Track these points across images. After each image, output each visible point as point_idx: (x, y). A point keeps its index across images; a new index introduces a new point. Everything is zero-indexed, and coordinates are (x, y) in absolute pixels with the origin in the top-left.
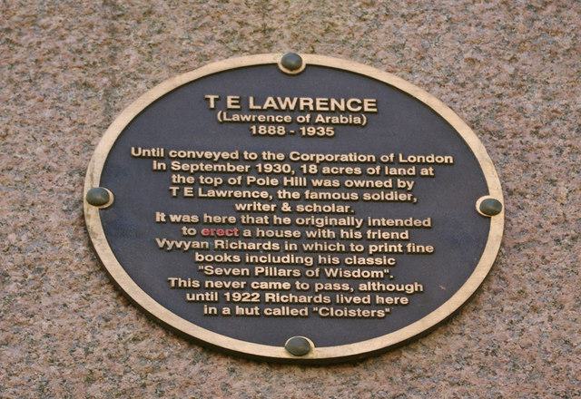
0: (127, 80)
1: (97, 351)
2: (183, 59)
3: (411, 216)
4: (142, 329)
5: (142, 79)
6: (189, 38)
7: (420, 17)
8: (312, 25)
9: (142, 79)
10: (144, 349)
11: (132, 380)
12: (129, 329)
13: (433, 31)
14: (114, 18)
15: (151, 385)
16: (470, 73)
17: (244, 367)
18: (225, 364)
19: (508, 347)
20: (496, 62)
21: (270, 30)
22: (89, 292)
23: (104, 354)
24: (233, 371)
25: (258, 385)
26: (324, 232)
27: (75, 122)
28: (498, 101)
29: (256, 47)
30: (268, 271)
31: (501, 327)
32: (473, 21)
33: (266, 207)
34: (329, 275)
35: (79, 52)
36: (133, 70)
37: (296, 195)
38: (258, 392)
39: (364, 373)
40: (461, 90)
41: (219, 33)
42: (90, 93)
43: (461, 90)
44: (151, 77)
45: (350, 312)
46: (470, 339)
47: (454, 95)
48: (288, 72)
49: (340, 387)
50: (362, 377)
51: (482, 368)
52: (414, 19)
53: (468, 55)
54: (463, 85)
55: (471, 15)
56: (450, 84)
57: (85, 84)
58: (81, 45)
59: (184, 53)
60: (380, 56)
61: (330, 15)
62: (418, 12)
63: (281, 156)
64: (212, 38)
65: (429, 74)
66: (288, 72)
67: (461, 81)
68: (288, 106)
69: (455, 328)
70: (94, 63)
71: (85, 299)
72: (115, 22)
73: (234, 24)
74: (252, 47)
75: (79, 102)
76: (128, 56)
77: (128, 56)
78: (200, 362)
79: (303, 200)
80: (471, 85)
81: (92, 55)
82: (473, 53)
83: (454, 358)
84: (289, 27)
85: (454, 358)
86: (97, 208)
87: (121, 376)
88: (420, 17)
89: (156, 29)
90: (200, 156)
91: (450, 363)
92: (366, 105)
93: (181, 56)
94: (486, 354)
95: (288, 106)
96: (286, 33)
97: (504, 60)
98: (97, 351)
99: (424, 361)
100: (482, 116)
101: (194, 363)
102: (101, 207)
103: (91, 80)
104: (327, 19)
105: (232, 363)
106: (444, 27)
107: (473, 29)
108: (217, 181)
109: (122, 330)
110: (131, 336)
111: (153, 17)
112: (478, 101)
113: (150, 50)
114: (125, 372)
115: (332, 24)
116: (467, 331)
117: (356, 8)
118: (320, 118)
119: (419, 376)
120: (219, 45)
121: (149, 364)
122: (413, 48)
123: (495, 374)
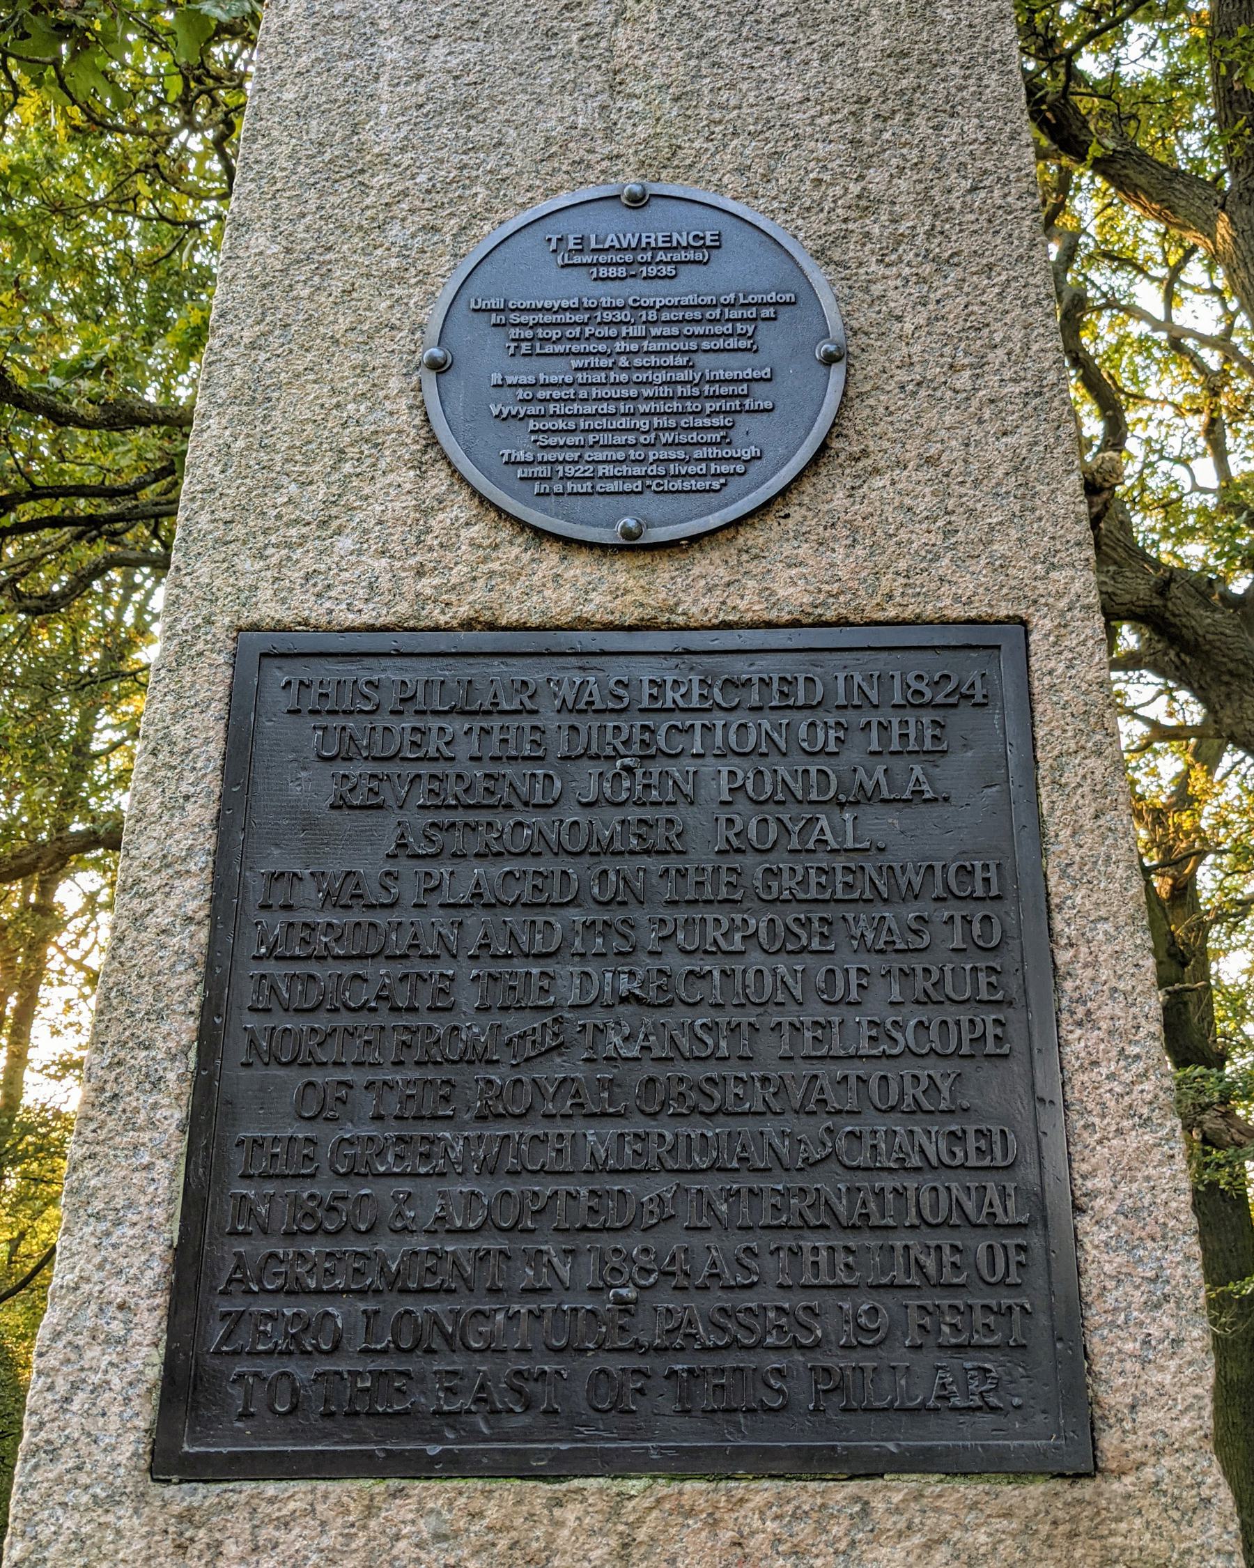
2: (530, 195)
6: (538, 172)
14: (465, 153)
30: (604, 438)
37: (634, 347)
47: (800, 222)
60: (725, 180)
63: (620, 302)
92: (708, 238)
101: (526, 550)
108: (554, 333)
115: (679, 147)
116: (806, 500)
118: (661, 256)
119: (756, 557)
123: (833, 550)
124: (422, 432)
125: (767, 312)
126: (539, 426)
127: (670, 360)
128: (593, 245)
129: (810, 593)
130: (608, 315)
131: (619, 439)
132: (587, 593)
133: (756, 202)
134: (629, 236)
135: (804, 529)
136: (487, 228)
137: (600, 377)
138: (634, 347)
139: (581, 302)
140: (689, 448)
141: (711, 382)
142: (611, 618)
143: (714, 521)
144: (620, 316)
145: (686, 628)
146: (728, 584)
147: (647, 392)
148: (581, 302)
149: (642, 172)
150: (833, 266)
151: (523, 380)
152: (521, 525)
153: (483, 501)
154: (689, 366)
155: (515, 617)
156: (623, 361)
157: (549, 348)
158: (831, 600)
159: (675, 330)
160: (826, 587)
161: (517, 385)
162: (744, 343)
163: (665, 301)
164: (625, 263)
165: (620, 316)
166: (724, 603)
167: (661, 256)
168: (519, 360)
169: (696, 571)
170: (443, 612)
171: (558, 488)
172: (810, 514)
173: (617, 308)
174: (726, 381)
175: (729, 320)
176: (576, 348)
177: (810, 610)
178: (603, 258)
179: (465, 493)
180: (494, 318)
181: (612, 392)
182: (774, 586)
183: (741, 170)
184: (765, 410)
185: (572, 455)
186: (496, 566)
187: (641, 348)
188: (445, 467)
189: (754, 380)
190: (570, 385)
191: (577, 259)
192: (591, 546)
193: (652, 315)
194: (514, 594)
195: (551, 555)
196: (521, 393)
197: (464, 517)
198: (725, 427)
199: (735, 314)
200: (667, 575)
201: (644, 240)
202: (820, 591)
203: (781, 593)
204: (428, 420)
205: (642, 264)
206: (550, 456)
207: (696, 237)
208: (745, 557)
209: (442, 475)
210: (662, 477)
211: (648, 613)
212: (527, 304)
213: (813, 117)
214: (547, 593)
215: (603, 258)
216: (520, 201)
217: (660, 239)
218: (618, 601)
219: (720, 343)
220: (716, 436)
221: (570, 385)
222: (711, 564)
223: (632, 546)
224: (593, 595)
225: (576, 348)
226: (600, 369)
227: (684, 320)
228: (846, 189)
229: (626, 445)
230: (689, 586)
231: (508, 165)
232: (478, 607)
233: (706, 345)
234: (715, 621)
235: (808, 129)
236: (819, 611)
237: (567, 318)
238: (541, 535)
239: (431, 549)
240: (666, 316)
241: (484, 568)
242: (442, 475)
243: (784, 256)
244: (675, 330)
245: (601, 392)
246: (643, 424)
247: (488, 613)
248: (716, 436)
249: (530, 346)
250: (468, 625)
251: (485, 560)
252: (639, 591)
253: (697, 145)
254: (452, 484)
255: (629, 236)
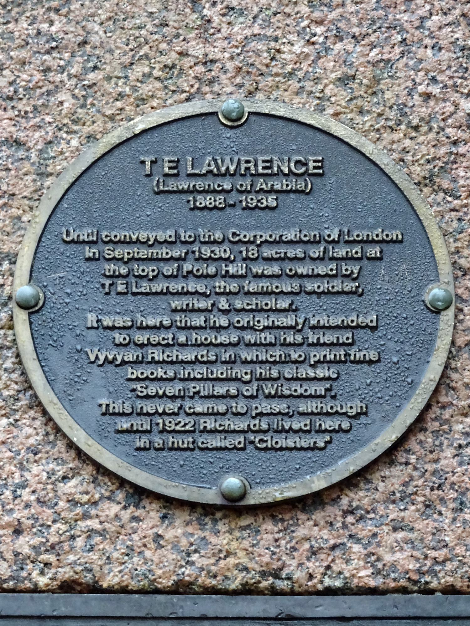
0: (59, 134)
1: (26, 494)
2: (119, 104)
3: (379, 226)
4: (71, 465)
5: (75, 132)
6: (126, 77)
7: (373, 38)
8: (258, 53)
9: (75, 132)
10: (73, 491)
11: (61, 532)
12: (58, 464)
13: (385, 57)
14: (48, 52)
15: (79, 536)
16: (424, 111)
17: (178, 512)
18: (158, 508)
19: (454, 479)
20: (455, 97)
21: (213, 61)
22: (17, 417)
23: (33, 498)
24: (164, 517)
25: (192, 535)
26: (263, 335)
27: (5, 192)
28: (454, 150)
29: (196, 86)
30: (204, 389)
31: (449, 452)
32: (427, 41)
33: (202, 304)
34: (267, 391)
35: (11, 98)
36: (66, 121)
37: (233, 286)
38: (192, 544)
39: (302, 517)
40: (414, 134)
41: (157, 68)
42: (21, 154)
43: (414, 134)
44: (86, 130)
45: (296, 337)
46: (415, 469)
47: (407, 143)
48: (229, 124)
49: (277, 536)
50: (300, 522)
51: (427, 506)
52: (366, 41)
53: (421, 89)
54: (416, 128)
55: (427, 33)
56: (403, 127)
57: (15, 141)
58: (12, 89)
59: (121, 96)
60: (328, 91)
61: (276, 39)
62: (370, 31)
63: (218, 236)
64: (150, 75)
65: (380, 115)
66: (229, 124)
67: (415, 122)
68: (228, 169)
69: (401, 457)
70: (26, 112)
71: (13, 425)
72: (46, 57)
73: (174, 55)
74: (192, 86)
75: (10, 166)
76: (61, 103)
77: (61, 103)
78: (131, 507)
79: (241, 292)
80: (424, 129)
81: (24, 101)
82: (428, 85)
83: (398, 495)
84: (232, 58)
85: (398, 495)
86: (27, 312)
87: (49, 526)
88: (373, 38)
89: (91, 65)
90: (134, 238)
91: (394, 502)
92: (311, 164)
93: (117, 100)
94: (432, 489)
95: (228, 169)
96: (230, 66)
97: (462, 93)
98: (26, 494)
99: (367, 499)
100: (436, 169)
101: (125, 508)
102: (31, 311)
103: (21, 135)
104: (273, 44)
105: (165, 507)
106: (398, 50)
107: (429, 52)
108: (150, 269)
109: (51, 466)
110: (60, 473)
111: (88, 48)
112: (432, 150)
113: (84, 93)
114: (54, 521)
115: (279, 51)
116: (413, 459)
117: (304, 28)
118: (260, 184)
119: (361, 518)
120: (158, 85)
121: (79, 510)
122: (365, 74)
123: (440, 514)
124: (14, 376)
125: (374, 251)
126: (137, 373)
127: (271, 302)
128: (190, 171)
129: (417, 559)
130: (206, 251)
131: (220, 390)
132: (189, 555)
133: (359, 119)
134: (227, 159)
135: (410, 490)
136: (75, 143)
137: (199, 320)
138: (233, 286)
139: (177, 235)
140: (292, 401)
141: (313, 328)
142: (214, 582)
143: (318, 483)
144: (219, 251)
145: (292, 593)
146: (334, 548)
147: (249, 337)
148: (177, 235)
149: (238, 80)
150: (441, 195)
151: (119, 323)
152: (122, 482)
153: (80, 454)
154: (291, 309)
155: (116, 580)
156: (223, 303)
157: (145, 286)
158: (437, 568)
159: (276, 269)
160: (433, 554)
161: (113, 328)
162: (350, 286)
163: (266, 237)
164: (223, 191)
165: (219, 251)
166: (328, 567)
167: (260, 184)
168: (113, 299)
169: (301, 532)
170: (42, 573)
171: (158, 441)
172: (416, 474)
173: (215, 242)
174: (330, 327)
175: (332, 259)
176: (176, 286)
177: (415, 577)
178: (200, 184)
179: (61, 445)
180: (89, 252)
181: (211, 336)
182: (381, 551)
183: (345, 80)
184: (370, 362)
185: (172, 406)
186: (94, 524)
187: (241, 288)
188: (39, 415)
189: (358, 327)
190: (168, 328)
191: (172, 184)
192: (191, 506)
193: (253, 252)
194: (116, 555)
195: (151, 516)
196: (119, 337)
197: (61, 471)
198: (329, 379)
199: (341, 252)
200: (270, 537)
201: (243, 166)
202: (426, 557)
203: (388, 558)
204: (20, 363)
205: (241, 192)
206: (149, 407)
207: (297, 162)
208: (350, 519)
209: (37, 423)
210: (265, 432)
211: (251, 577)
212: (121, 235)
213: (422, 19)
214: (148, 554)
215: (200, 184)
216: (109, 112)
217: (260, 165)
218: (222, 563)
219: (325, 286)
220: (320, 389)
221: (168, 328)
222: (311, 529)
223: (234, 508)
224: (195, 557)
225: (176, 286)
226: (199, 310)
227: (286, 258)
228: (456, 106)
229: (227, 396)
230: (294, 549)
231: (95, 68)
232: (79, 568)
233: (310, 286)
234: (320, 587)
235: (417, 33)
236: (428, 578)
237: (163, 252)
238: (139, 494)
239: (27, 506)
240: (267, 252)
241: (83, 525)
242: (37, 423)
243: (399, 192)
244: (276, 269)
245: (201, 337)
246: (239, 371)
247: (89, 576)
248: (320, 389)
249: (124, 283)
250: (68, 587)
251: (86, 516)
252: (241, 554)
253: (297, 48)
254: (47, 434)
255: (227, 159)
